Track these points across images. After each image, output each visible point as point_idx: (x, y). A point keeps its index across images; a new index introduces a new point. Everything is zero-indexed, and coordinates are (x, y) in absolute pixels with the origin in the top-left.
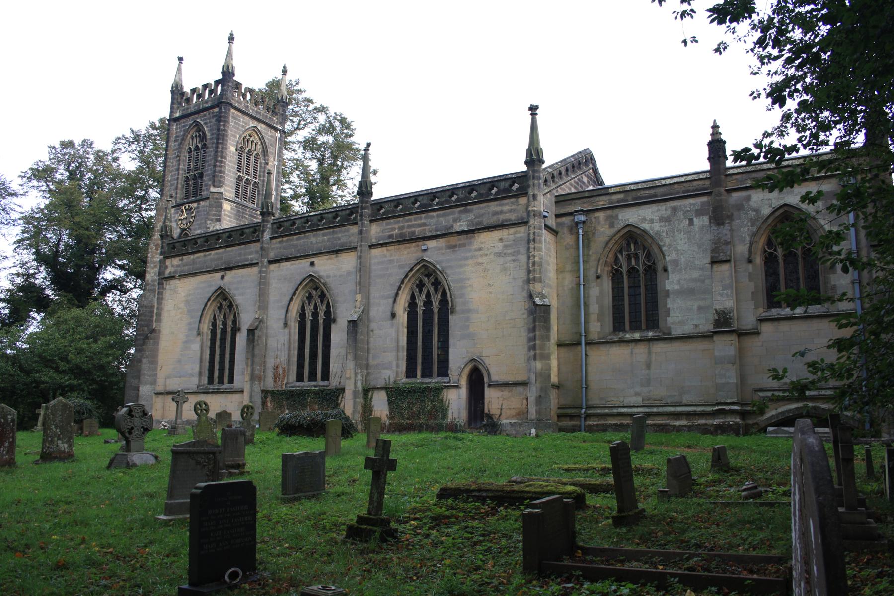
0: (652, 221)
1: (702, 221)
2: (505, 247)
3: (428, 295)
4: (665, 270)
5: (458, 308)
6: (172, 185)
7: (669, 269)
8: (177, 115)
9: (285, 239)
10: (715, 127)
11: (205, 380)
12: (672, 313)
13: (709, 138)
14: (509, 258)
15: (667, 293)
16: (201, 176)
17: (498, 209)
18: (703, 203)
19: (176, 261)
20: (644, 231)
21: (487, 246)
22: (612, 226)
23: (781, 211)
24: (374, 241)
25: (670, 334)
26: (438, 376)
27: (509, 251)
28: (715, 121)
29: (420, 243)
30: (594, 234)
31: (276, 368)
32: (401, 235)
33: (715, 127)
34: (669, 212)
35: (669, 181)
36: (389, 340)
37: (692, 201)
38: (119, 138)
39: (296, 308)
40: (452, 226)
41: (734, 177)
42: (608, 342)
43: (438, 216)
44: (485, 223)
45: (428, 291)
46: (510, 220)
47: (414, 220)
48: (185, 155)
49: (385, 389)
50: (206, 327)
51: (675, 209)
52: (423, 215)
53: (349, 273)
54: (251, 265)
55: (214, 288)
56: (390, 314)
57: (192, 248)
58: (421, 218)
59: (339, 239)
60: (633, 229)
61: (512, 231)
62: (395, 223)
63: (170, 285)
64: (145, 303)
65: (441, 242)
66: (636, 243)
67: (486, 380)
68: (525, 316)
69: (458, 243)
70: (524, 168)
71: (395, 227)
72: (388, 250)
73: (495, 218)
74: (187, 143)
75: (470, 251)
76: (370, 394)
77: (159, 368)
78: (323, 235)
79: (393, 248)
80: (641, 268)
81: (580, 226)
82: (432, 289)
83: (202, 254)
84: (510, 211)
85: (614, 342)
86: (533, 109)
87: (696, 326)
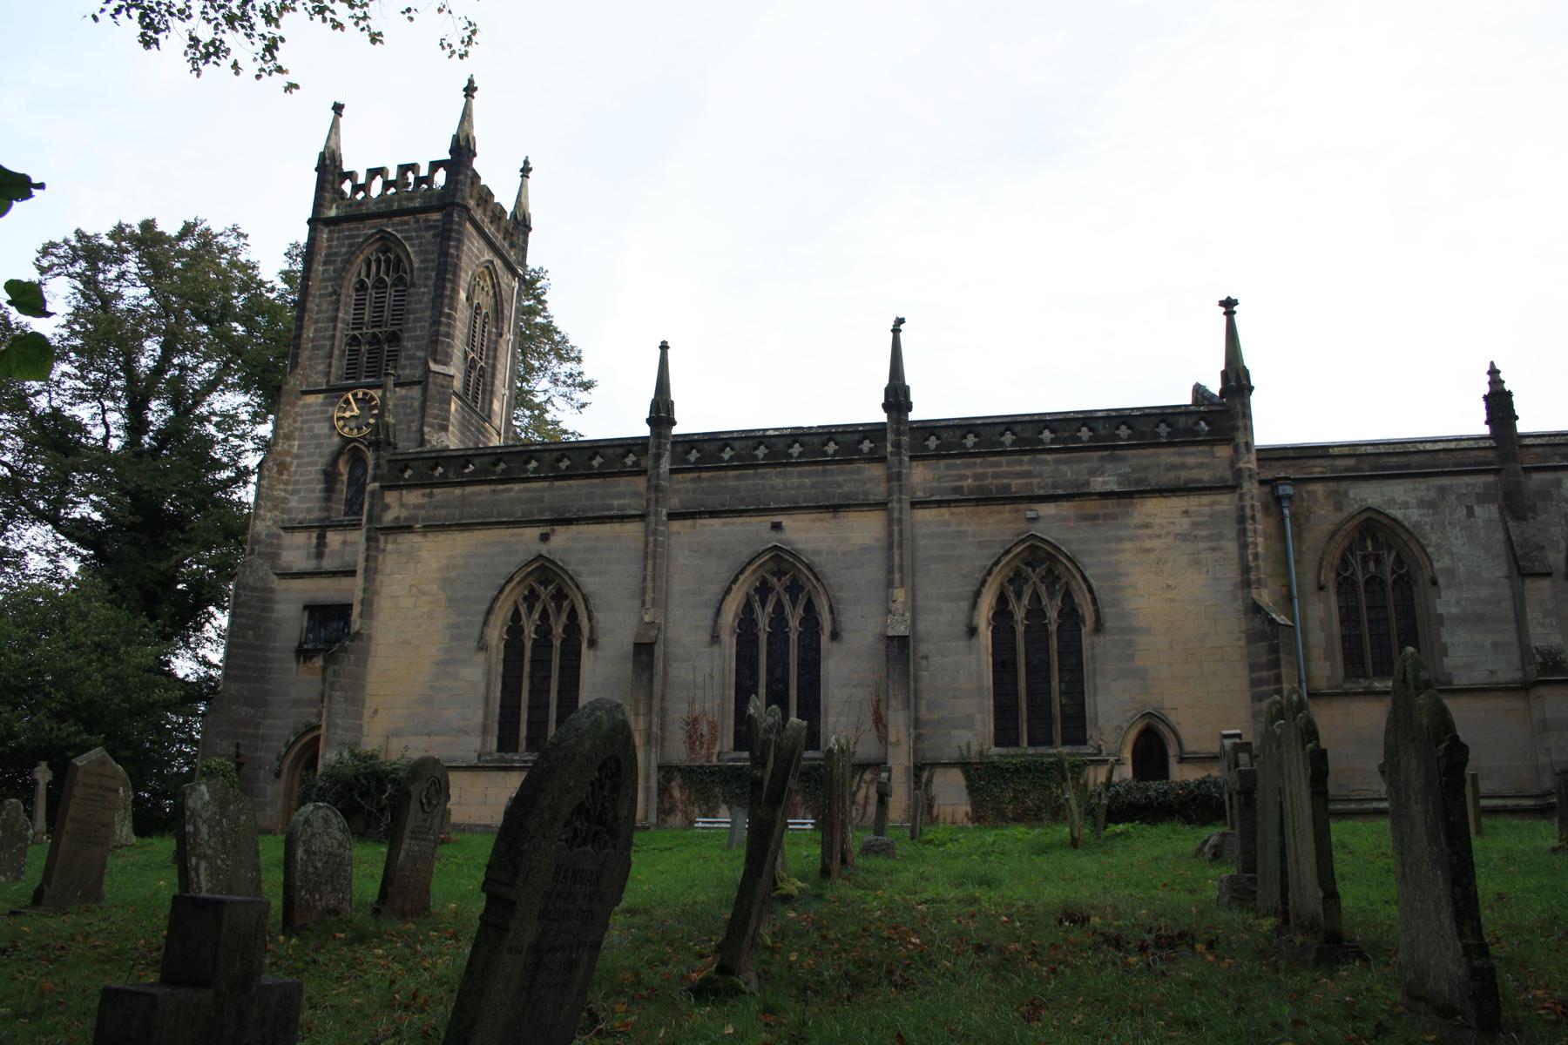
0: (1406, 505)
1: (1487, 513)
2: (1195, 525)
3: (544, 615)
4: (1434, 583)
5: (1108, 625)
6: (315, 348)
7: (1441, 581)
8: (333, 213)
9: (705, 475)
10: (1494, 372)
11: (493, 743)
12: (1451, 652)
13: (1486, 390)
14: (1203, 545)
15: (1440, 620)
16: (394, 338)
17: (1178, 460)
18: (1486, 485)
19: (414, 497)
20: (1394, 520)
21: (1158, 521)
22: (1338, 507)
23: (1363, 517)
24: (920, 495)
25: (1451, 683)
26: (1064, 743)
27: (1204, 533)
28: (1492, 364)
29: (1023, 507)
30: (1307, 519)
31: (693, 722)
32: (980, 489)
33: (1494, 372)
34: (1432, 494)
35: (1429, 447)
36: (962, 676)
37: (1468, 479)
38: (54, 245)
39: (734, 608)
40: (1088, 483)
41: (1533, 450)
42: (1346, 694)
43: (1056, 462)
44: (1153, 482)
45: (779, 600)
46: (1200, 481)
47: (1005, 465)
48: (349, 294)
49: (964, 765)
50: (496, 635)
51: (1442, 490)
52: (1026, 458)
53: (865, 549)
54: (622, 518)
55: (521, 558)
56: (965, 629)
57: (458, 475)
58: (1021, 463)
59: (840, 486)
60: (1375, 516)
61: (1205, 499)
62: (968, 466)
63: (393, 547)
64: (251, 580)
65: (1067, 508)
66: (1374, 538)
67: (1172, 750)
68: (1242, 643)
69: (1102, 512)
70: (645, 431)
71: (968, 474)
72: (952, 514)
73: (1172, 475)
74: (355, 269)
75: (1127, 527)
76: (925, 775)
77: (367, 713)
78: (800, 475)
79: (963, 510)
80: (1389, 578)
81: (1285, 503)
82: (786, 598)
83: (486, 488)
84: (1201, 466)
85: (1357, 694)
86: (1229, 305)
87: (1493, 673)
